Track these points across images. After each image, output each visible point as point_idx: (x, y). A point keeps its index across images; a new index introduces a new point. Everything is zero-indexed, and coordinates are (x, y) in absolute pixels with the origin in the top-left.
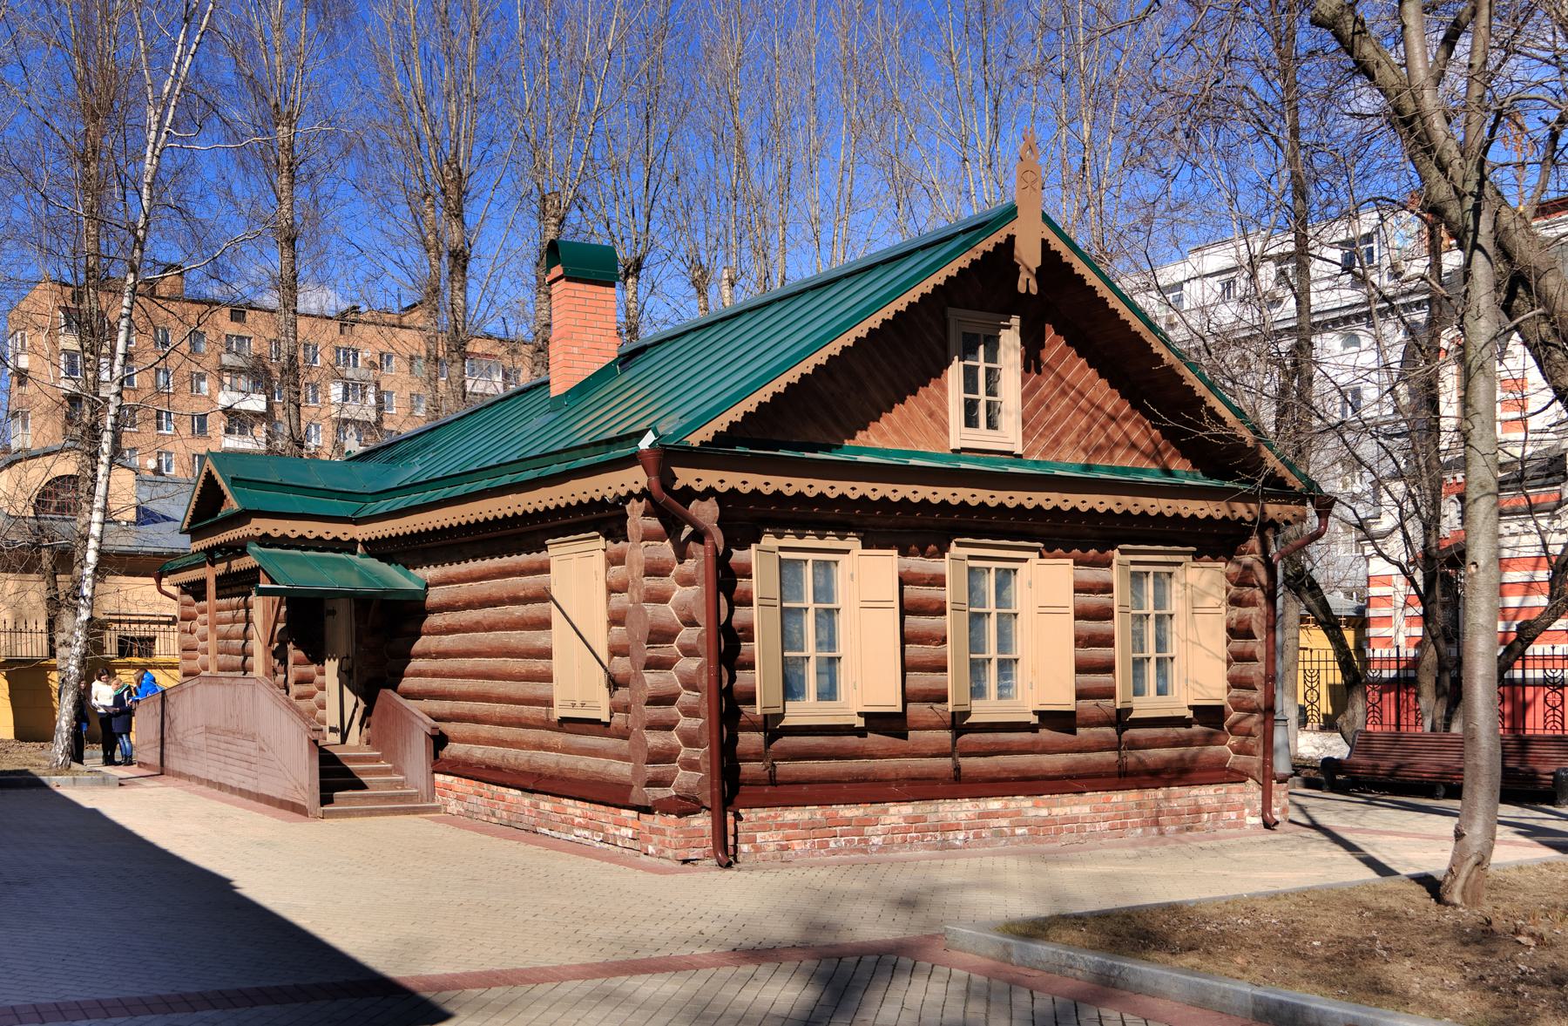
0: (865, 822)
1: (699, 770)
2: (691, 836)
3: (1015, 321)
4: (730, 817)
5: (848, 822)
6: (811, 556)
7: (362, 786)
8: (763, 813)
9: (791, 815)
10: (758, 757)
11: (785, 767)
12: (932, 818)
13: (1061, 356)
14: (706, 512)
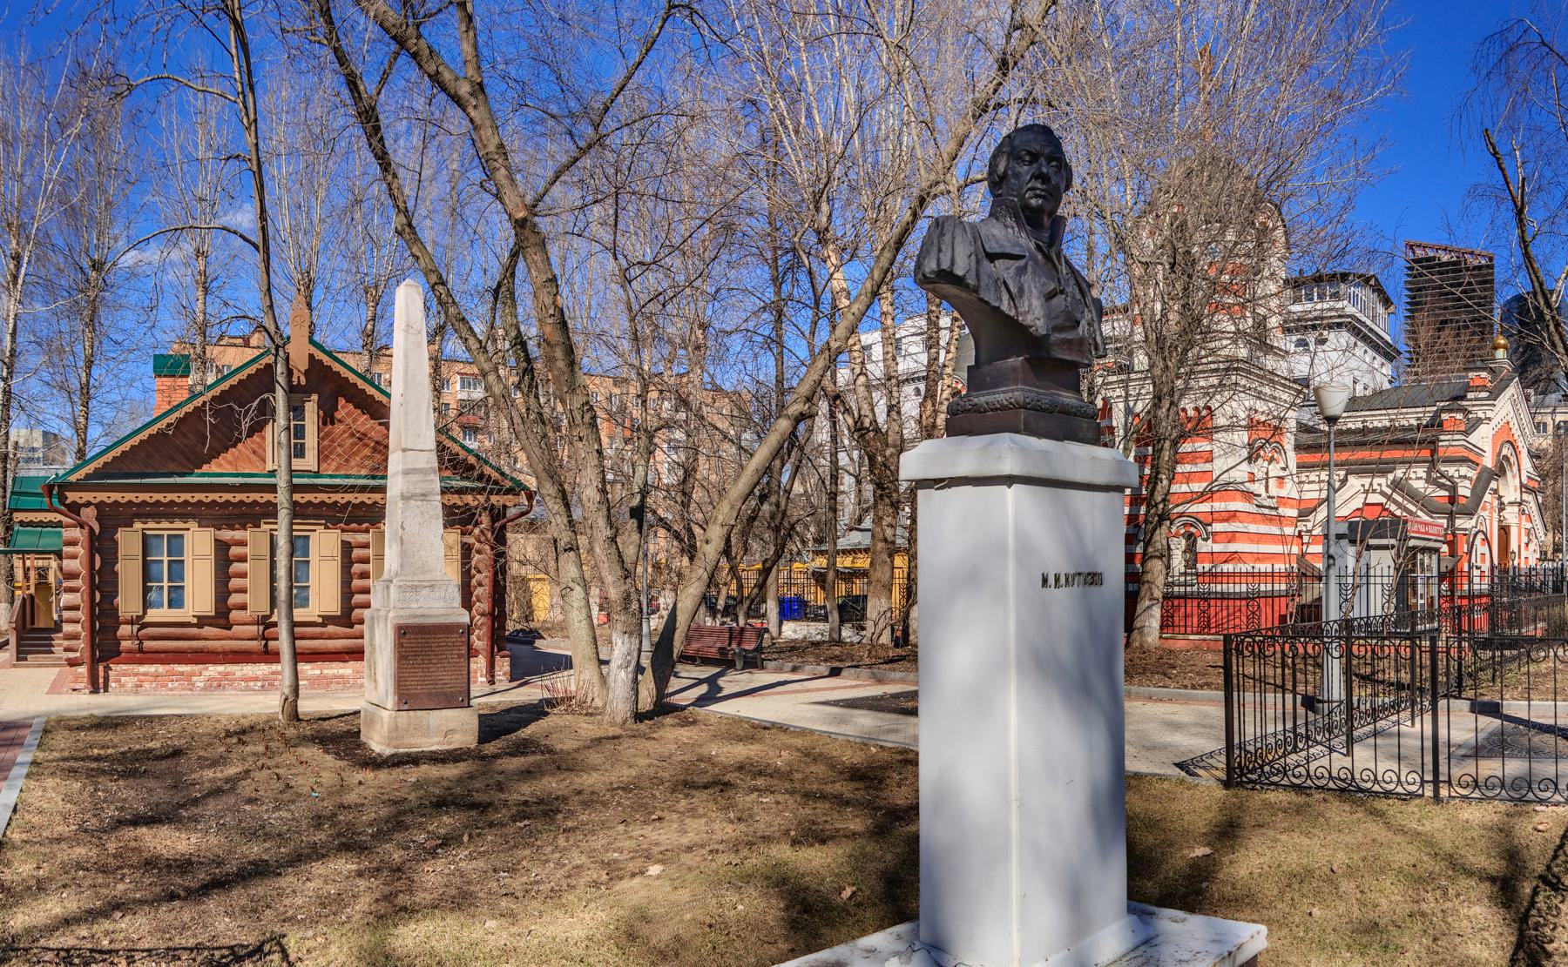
0: (192, 674)
1: (825, 619)
2: (76, 679)
3: (315, 397)
4: (101, 668)
5: (182, 674)
6: (166, 533)
7: (1320, 599)
8: (125, 667)
9: (143, 669)
10: (130, 638)
11: (148, 644)
12: (239, 674)
13: (349, 414)
14: (89, 514)
